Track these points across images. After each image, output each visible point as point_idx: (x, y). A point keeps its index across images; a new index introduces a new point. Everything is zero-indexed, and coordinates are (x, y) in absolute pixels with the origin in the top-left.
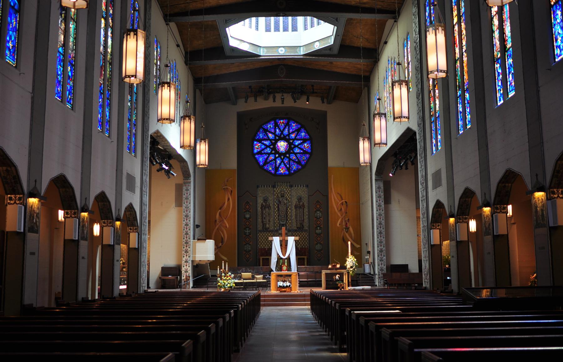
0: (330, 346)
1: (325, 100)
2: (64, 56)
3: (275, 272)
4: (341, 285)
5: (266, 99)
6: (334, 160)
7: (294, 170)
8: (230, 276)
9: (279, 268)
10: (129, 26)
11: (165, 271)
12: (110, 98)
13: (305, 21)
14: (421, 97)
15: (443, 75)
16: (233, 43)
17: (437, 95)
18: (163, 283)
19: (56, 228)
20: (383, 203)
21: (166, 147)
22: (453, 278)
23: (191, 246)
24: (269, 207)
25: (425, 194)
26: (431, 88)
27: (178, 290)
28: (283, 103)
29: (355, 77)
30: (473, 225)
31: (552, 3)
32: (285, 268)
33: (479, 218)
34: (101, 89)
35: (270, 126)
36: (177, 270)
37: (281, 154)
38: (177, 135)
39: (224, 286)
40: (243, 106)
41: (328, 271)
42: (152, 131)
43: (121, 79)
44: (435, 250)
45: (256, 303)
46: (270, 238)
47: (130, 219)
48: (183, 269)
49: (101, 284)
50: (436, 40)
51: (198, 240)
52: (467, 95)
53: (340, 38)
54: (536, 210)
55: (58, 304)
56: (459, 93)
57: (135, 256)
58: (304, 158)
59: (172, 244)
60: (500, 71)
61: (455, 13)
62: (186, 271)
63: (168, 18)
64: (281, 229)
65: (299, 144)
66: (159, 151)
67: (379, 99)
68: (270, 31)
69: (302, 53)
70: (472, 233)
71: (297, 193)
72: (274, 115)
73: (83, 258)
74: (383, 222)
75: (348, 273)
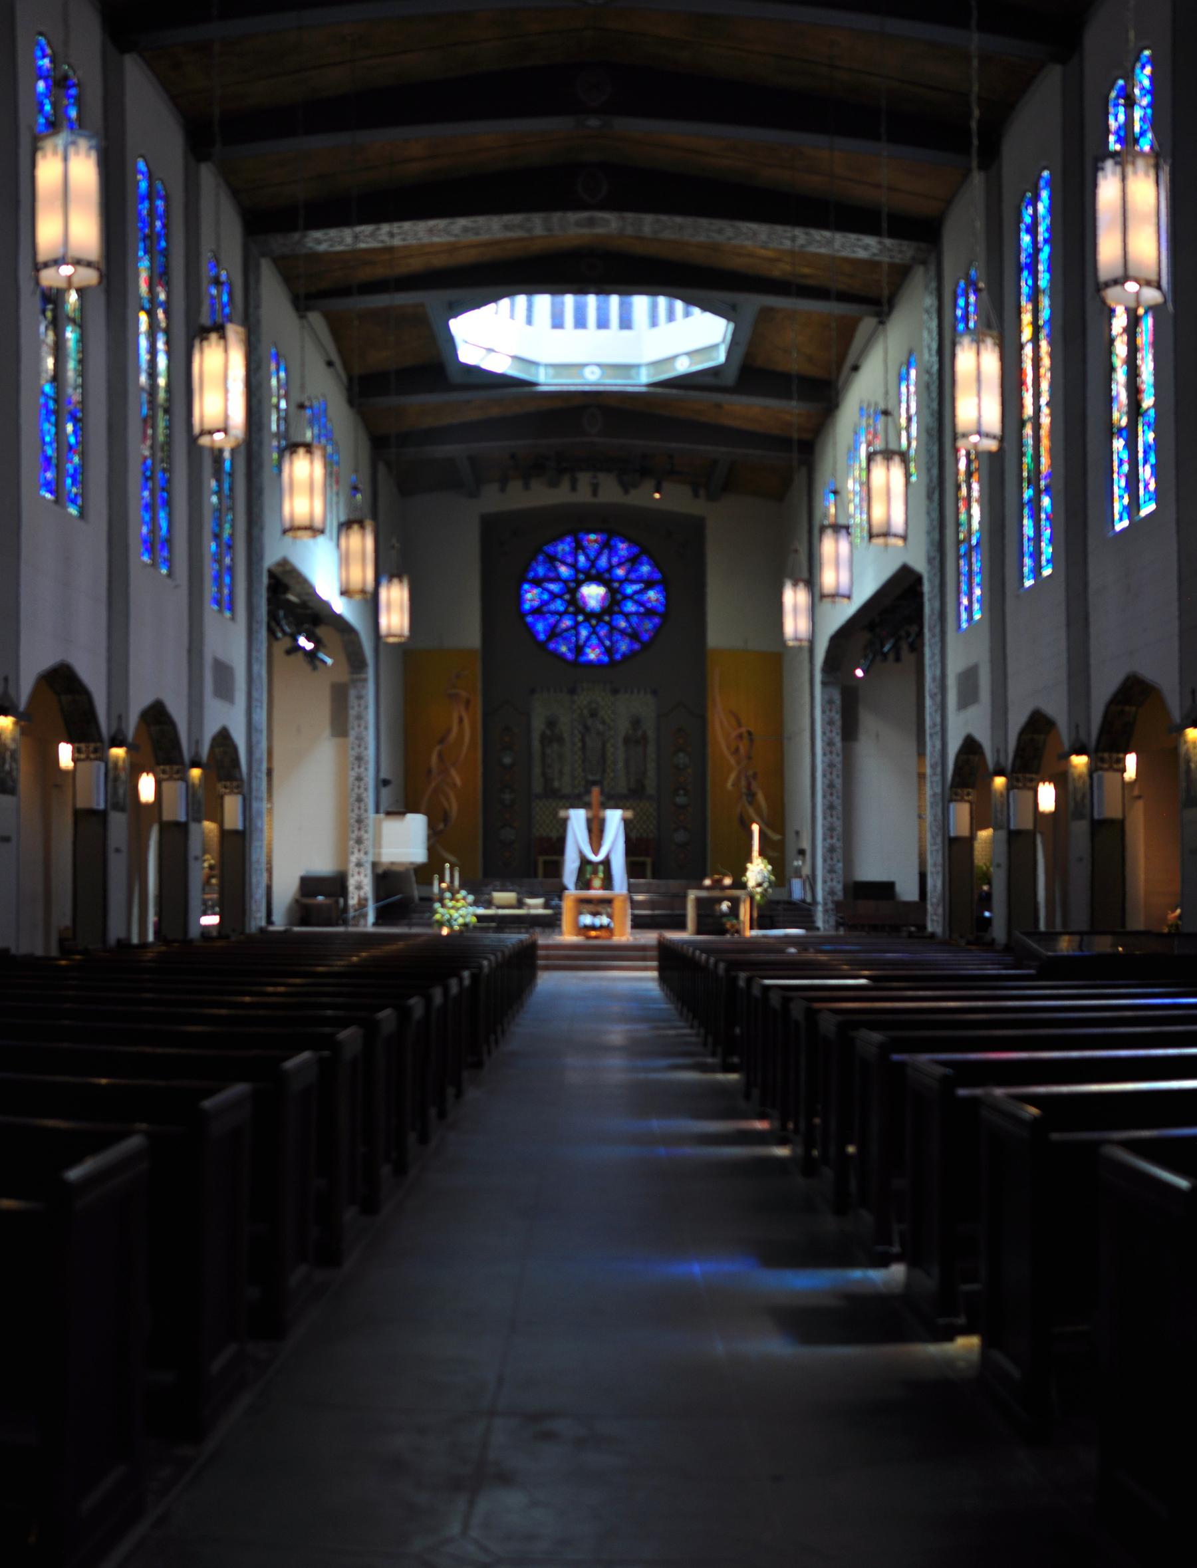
0: (700, 1059)
1: (702, 492)
2: (56, 401)
3: (572, 892)
4: (733, 926)
5: (554, 484)
6: (721, 631)
7: (624, 655)
8: (464, 898)
9: (583, 882)
10: (205, 320)
11: (310, 885)
12: (167, 486)
13: (654, 308)
14: (937, 492)
15: (992, 445)
16: (467, 355)
17: (975, 493)
18: (303, 912)
19: (56, 786)
21: (306, 598)
22: (996, 915)
23: (371, 829)
24: (560, 740)
25: (938, 720)
26: (962, 477)
27: (341, 929)
28: (595, 493)
29: (779, 442)
30: (1047, 797)
32: (597, 883)
33: (1061, 781)
34: (146, 469)
35: (563, 548)
36: (337, 885)
37: (590, 615)
38: (331, 569)
39: (449, 921)
40: (494, 500)
41: (703, 894)
42: (270, 559)
43: (192, 440)
44: (957, 849)
45: (526, 961)
46: (562, 814)
47: (224, 763)
48: (352, 882)
49: (160, 913)
50: (978, 364)
51: (388, 813)
52: (1046, 501)
53: (741, 351)
55: (65, 951)
56: (1028, 494)
57: (237, 848)
58: (648, 625)
59: (323, 823)
61: (1027, 318)
62: (359, 887)
63: (302, 303)
64: (588, 792)
65: (636, 592)
66: (288, 606)
67: (835, 493)
70: (1044, 816)
71: (629, 709)
72: (574, 523)
73: (118, 850)
74: (838, 782)
75: (752, 898)
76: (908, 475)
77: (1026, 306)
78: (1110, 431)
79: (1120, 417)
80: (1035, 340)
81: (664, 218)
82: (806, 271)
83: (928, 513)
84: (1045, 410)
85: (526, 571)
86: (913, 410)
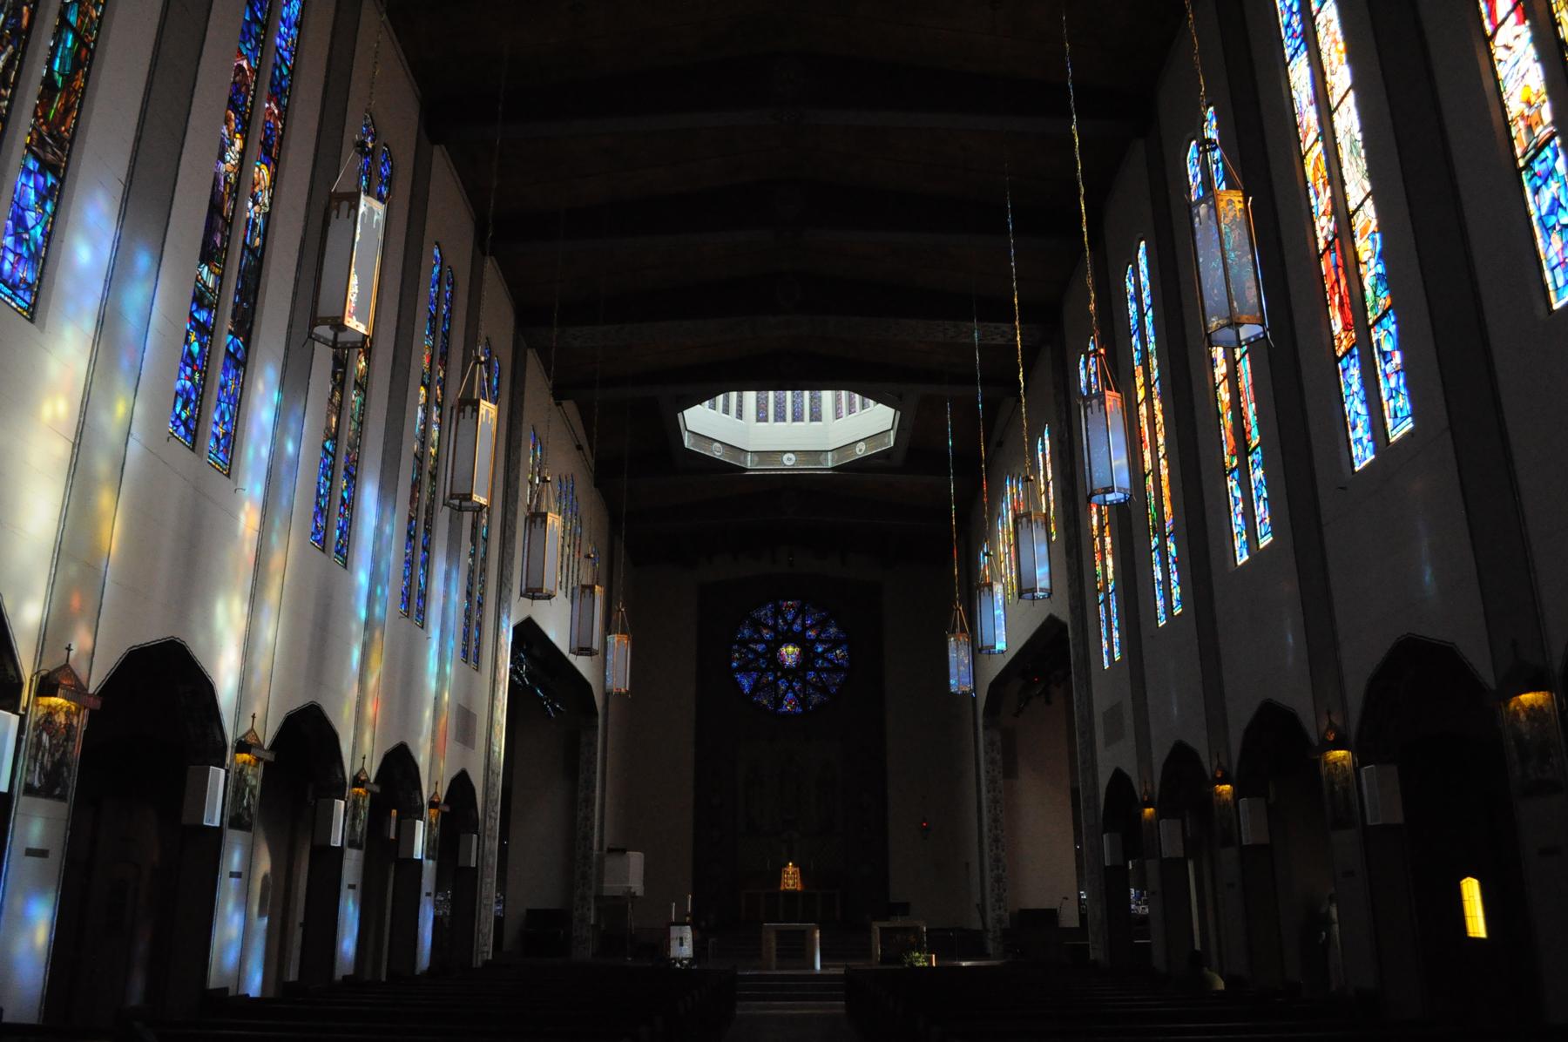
13: (838, 400)
17: (1109, 547)
26: (1096, 533)
31: (1340, 354)
37: (788, 673)
56: (1155, 542)
60: (1238, 494)
61: (1140, 381)
63: (559, 394)
68: (766, 420)
69: (830, 465)
73: (352, 887)
76: (1049, 535)
77: (1139, 370)
78: (1224, 473)
79: (1231, 461)
80: (1149, 398)
84: (1163, 462)
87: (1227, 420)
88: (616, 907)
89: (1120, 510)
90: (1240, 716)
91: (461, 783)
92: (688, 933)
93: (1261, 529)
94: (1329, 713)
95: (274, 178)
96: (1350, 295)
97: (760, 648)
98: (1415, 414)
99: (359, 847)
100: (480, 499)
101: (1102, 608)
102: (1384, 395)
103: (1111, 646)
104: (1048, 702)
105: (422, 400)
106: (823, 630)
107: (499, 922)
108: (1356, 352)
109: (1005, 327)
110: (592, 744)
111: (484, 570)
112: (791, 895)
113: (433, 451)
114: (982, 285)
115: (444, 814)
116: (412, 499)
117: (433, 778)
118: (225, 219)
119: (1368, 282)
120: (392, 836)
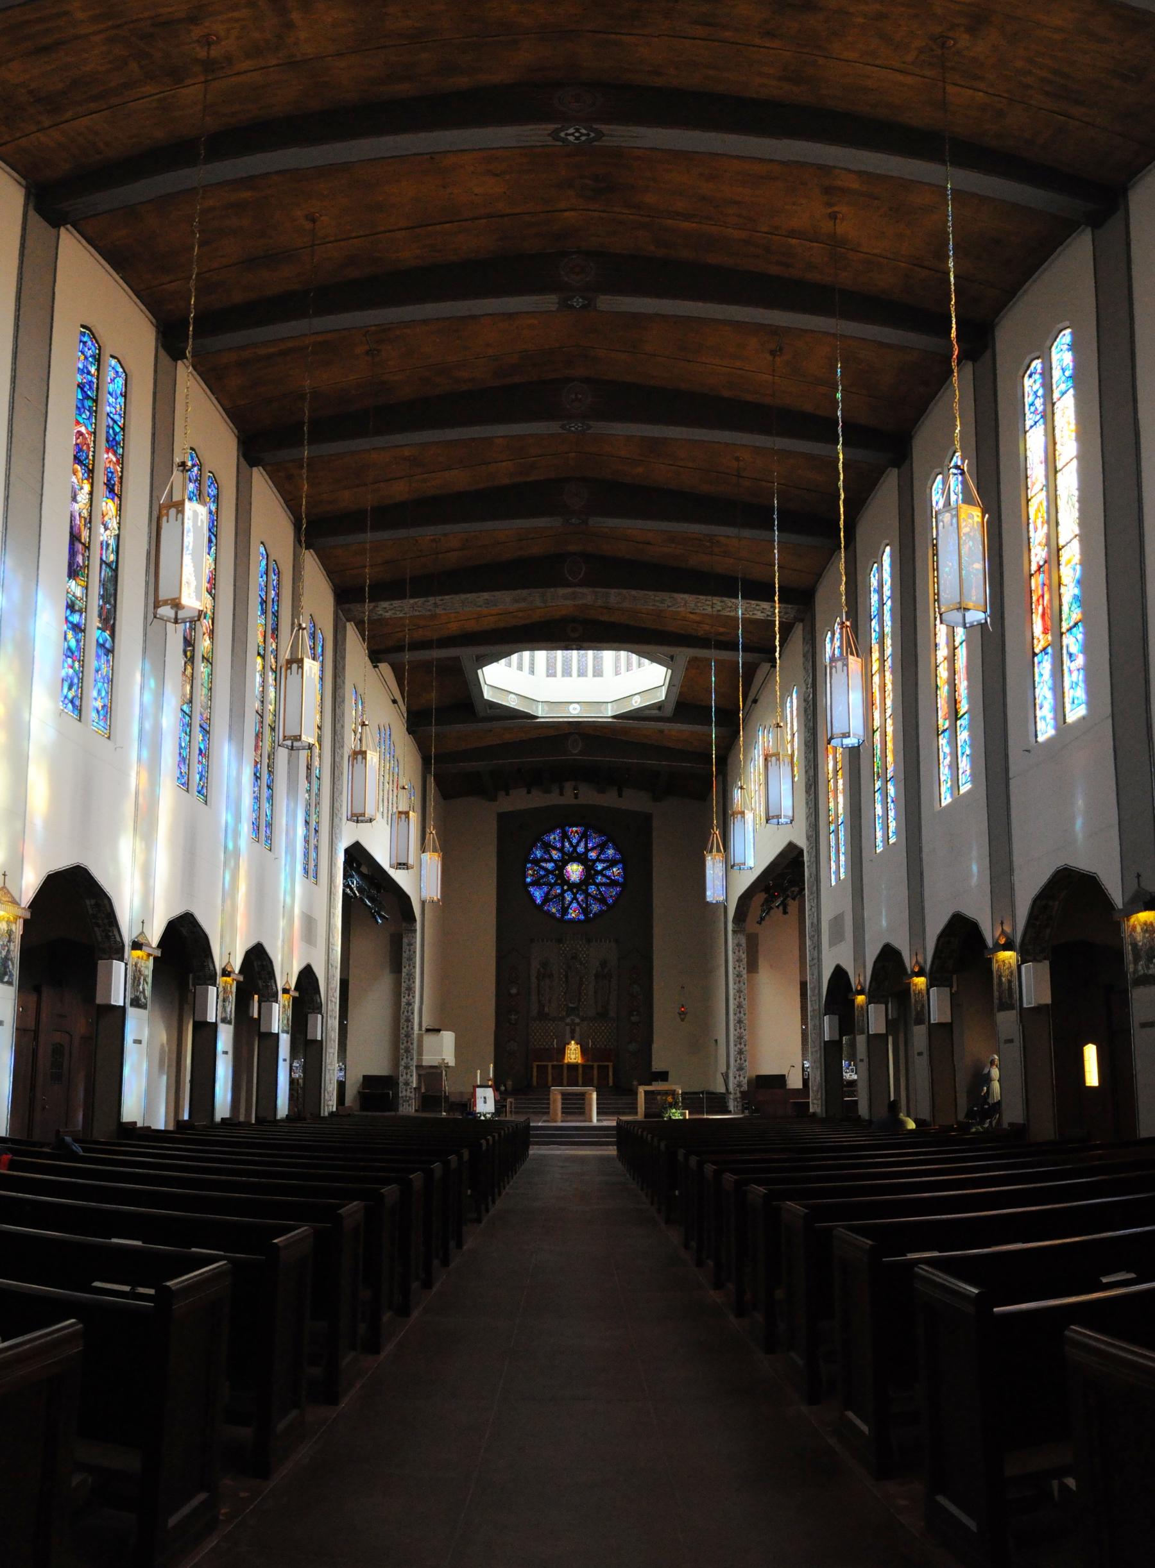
13: (617, 659)
17: (840, 787)
20: (745, 972)
26: (831, 776)
37: (572, 886)
53: (676, 690)
54: (1000, 980)
56: (878, 784)
60: (947, 750)
63: (375, 657)
68: (554, 675)
69: (610, 714)
72: (562, 818)
73: (226, 1053)
77: (875, 647)
79: (944, 724)
81: (624, 591)
82: (722, 630)
83: (807, 803)
84: (889, 722)
85: (529, 854)
86: (795, 728)
87: (944, 692)
88: (432, 1075)
89: (854, 753)
90: (935, 925)
91: (307, 976)
92: (489, 1093)
93: (963, 779)
94: (1002, 923)
95: (120, 509)
96: (1051, 608)
97: (550, 866)
98: (1090, 703)
99: (229, 1023)
100: (309, 738)
101: (832, 836)
102: (1067, 685)
103: (836, 868)
104: (785, 912)
105: (259, 667)
106: (602, 852)
107: (341, 1085)
108: (1049, 650)
109: (765, 605)
110: (411, 944)
111: (318, 804)
112: (573, 1067)
113: (271, 708)
114: (753, 535)
115: (294, 998)
116: (256, 747)
117: (286, 974)
118: (84, 544)
119: (1067, 599)
120: (256, 1016)
